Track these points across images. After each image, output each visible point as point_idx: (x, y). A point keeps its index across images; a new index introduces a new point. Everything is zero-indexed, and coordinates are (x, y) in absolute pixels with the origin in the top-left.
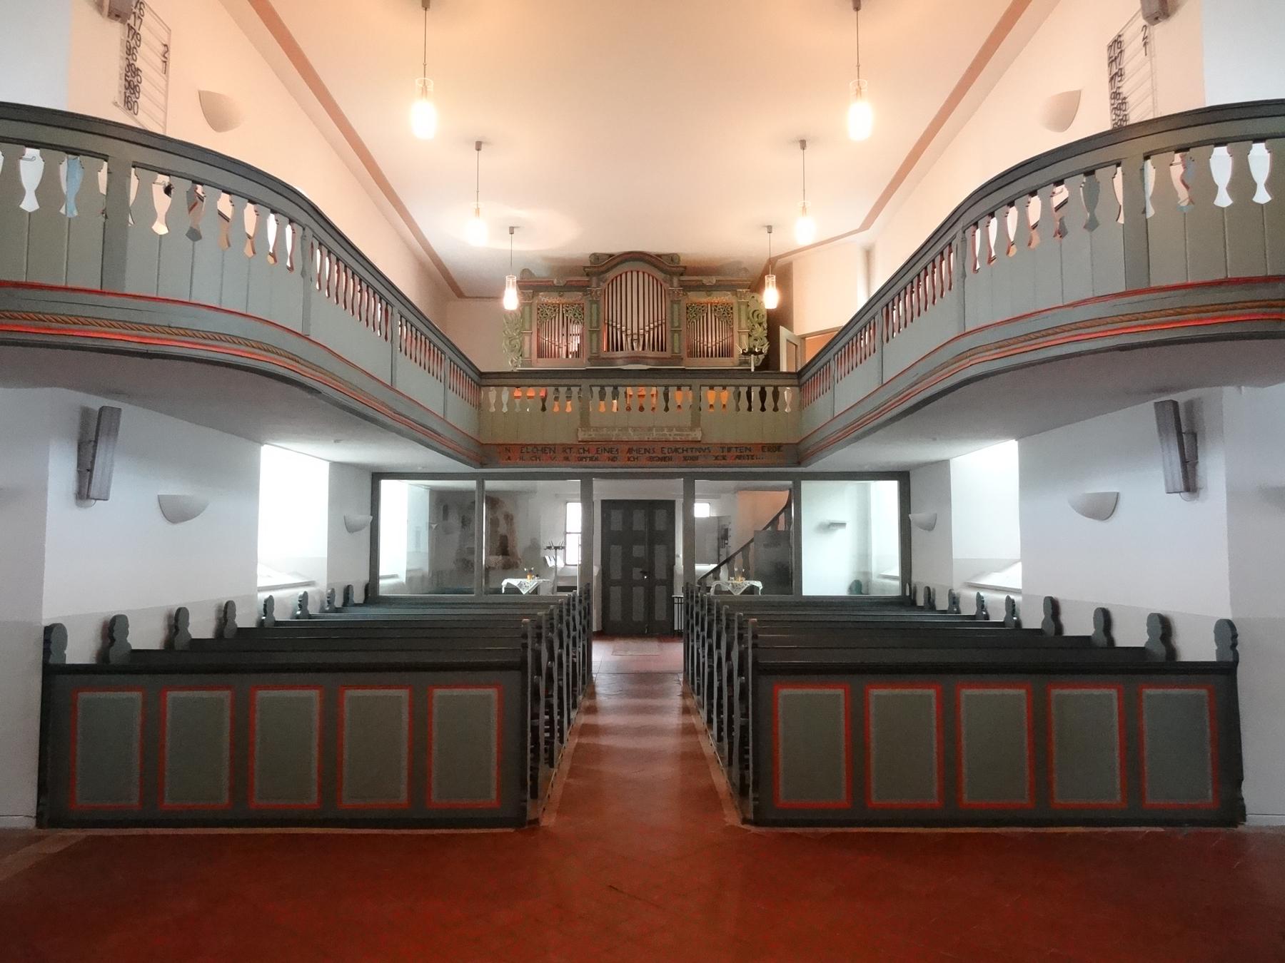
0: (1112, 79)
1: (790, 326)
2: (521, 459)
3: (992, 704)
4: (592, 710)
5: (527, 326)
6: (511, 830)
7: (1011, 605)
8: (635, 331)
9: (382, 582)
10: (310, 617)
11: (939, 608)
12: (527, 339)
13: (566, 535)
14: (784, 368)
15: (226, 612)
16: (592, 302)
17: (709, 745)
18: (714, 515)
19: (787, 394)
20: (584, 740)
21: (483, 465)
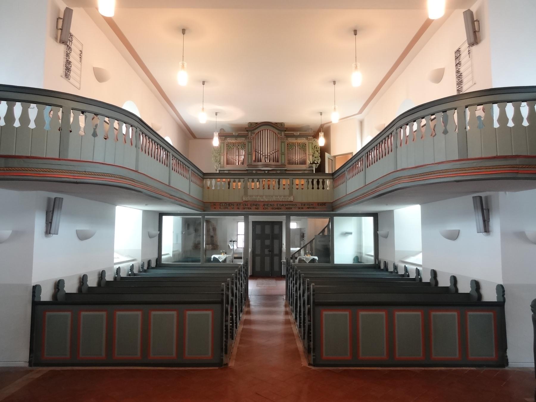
0: (456, 65)
1: (329, 152)
2: (220, 208)
3: (408, 318)
4: (249, 313)
5: (222, 152)
6: (217, 368)
7: (418, 271)
8: (266, 154)
9: (163, 257)
10: (135, 275)
11: (389, 270)
12: (222, 157)
13: (238, 235)
14: (327, 172)
15: (102, 275)
16: (249, 142)
17: (295, 330)
18: (299, 227)
19: (328, 182)
20: (246, 327)
21: (204, 211)
